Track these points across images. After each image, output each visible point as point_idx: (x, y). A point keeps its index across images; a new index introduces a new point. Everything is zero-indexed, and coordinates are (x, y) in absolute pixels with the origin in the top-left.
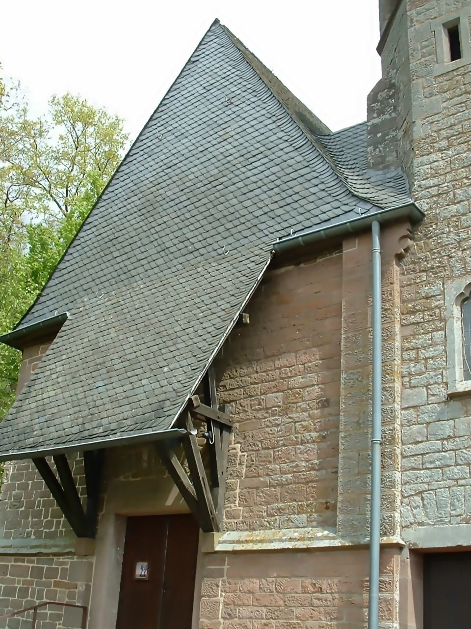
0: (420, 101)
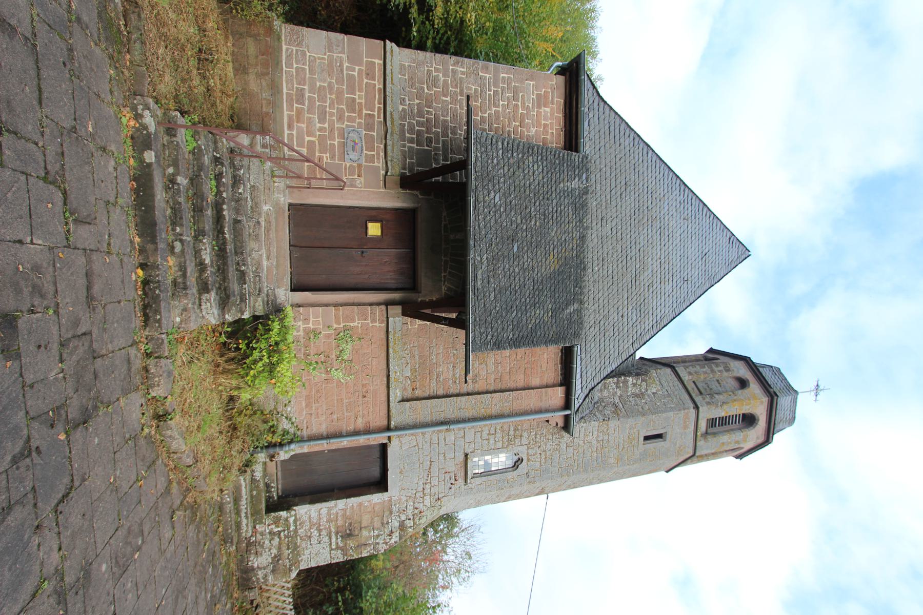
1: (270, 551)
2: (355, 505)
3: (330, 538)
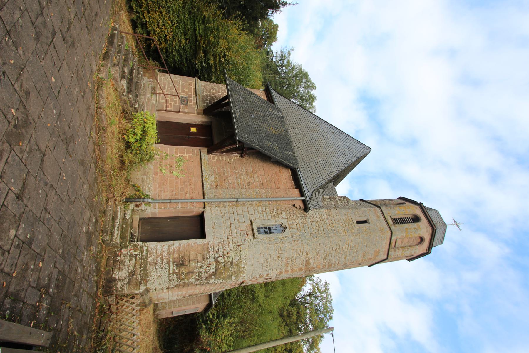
0: (343, 211)
1: (128, 268)
2: (186, 245)
3: (169, 265)
